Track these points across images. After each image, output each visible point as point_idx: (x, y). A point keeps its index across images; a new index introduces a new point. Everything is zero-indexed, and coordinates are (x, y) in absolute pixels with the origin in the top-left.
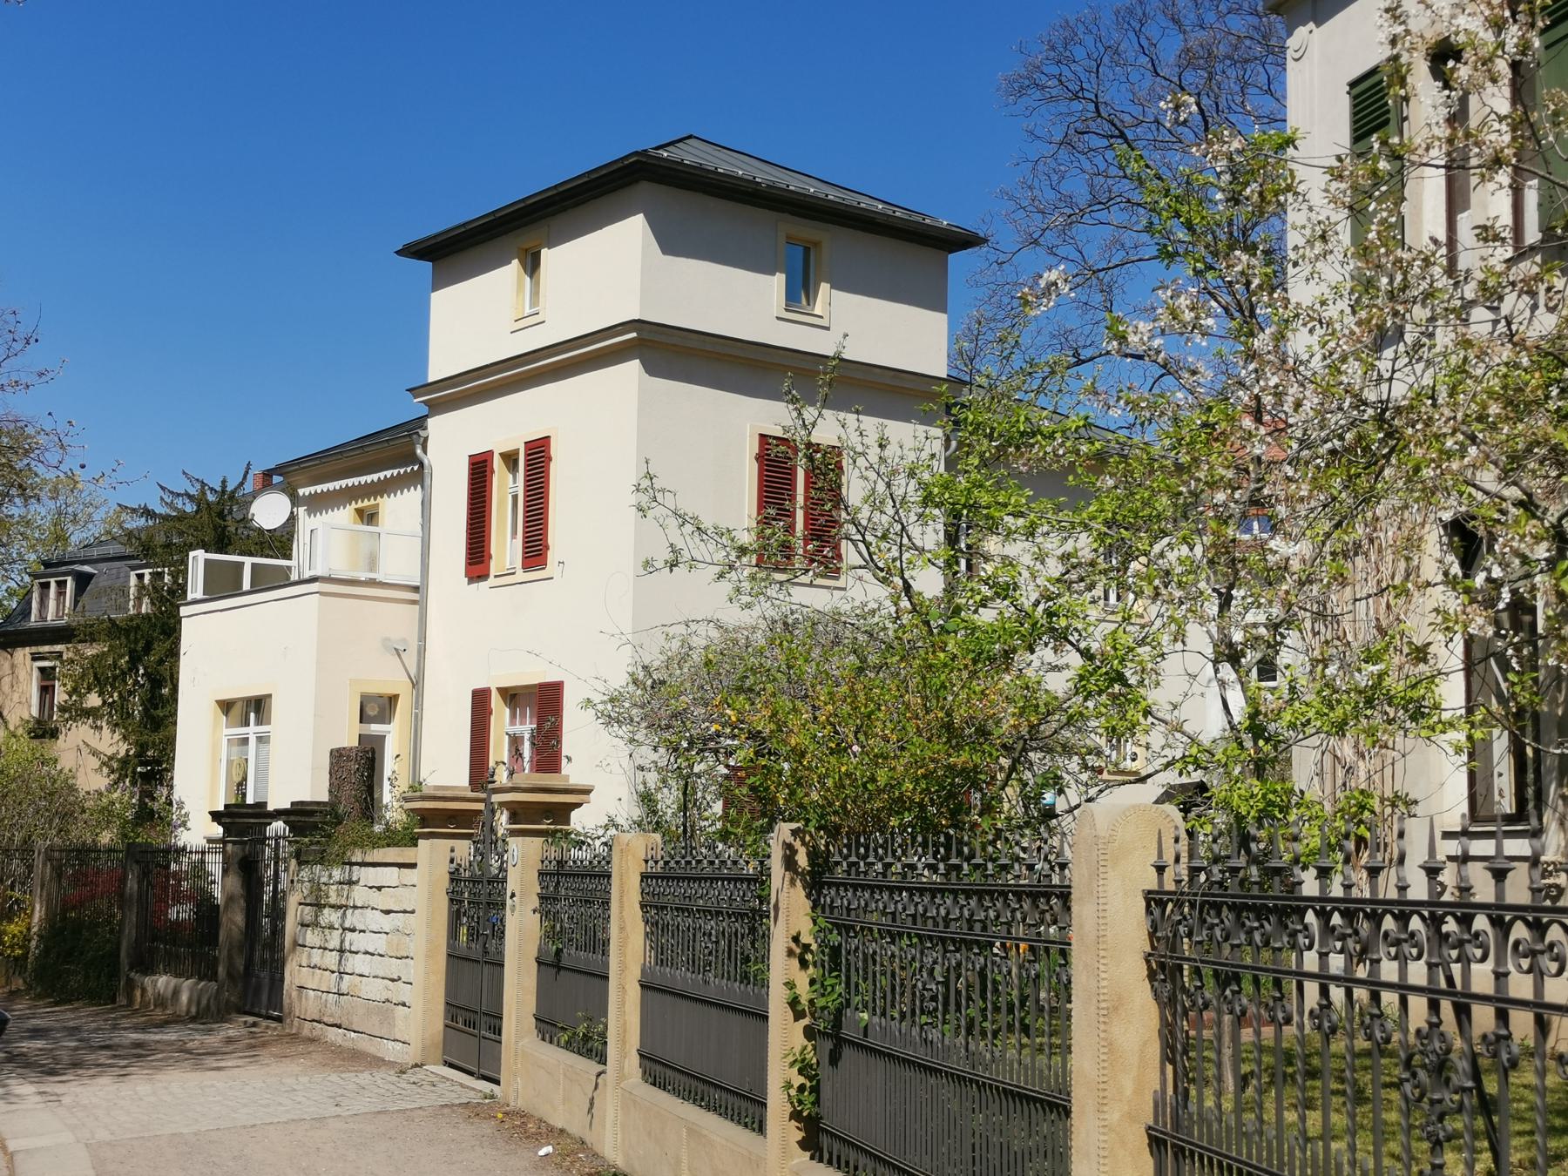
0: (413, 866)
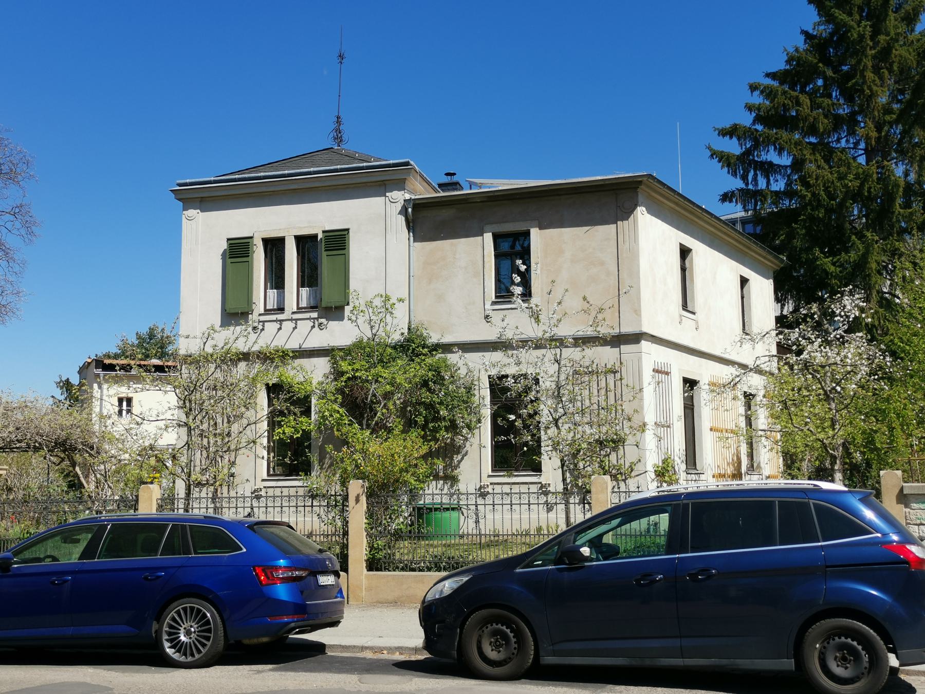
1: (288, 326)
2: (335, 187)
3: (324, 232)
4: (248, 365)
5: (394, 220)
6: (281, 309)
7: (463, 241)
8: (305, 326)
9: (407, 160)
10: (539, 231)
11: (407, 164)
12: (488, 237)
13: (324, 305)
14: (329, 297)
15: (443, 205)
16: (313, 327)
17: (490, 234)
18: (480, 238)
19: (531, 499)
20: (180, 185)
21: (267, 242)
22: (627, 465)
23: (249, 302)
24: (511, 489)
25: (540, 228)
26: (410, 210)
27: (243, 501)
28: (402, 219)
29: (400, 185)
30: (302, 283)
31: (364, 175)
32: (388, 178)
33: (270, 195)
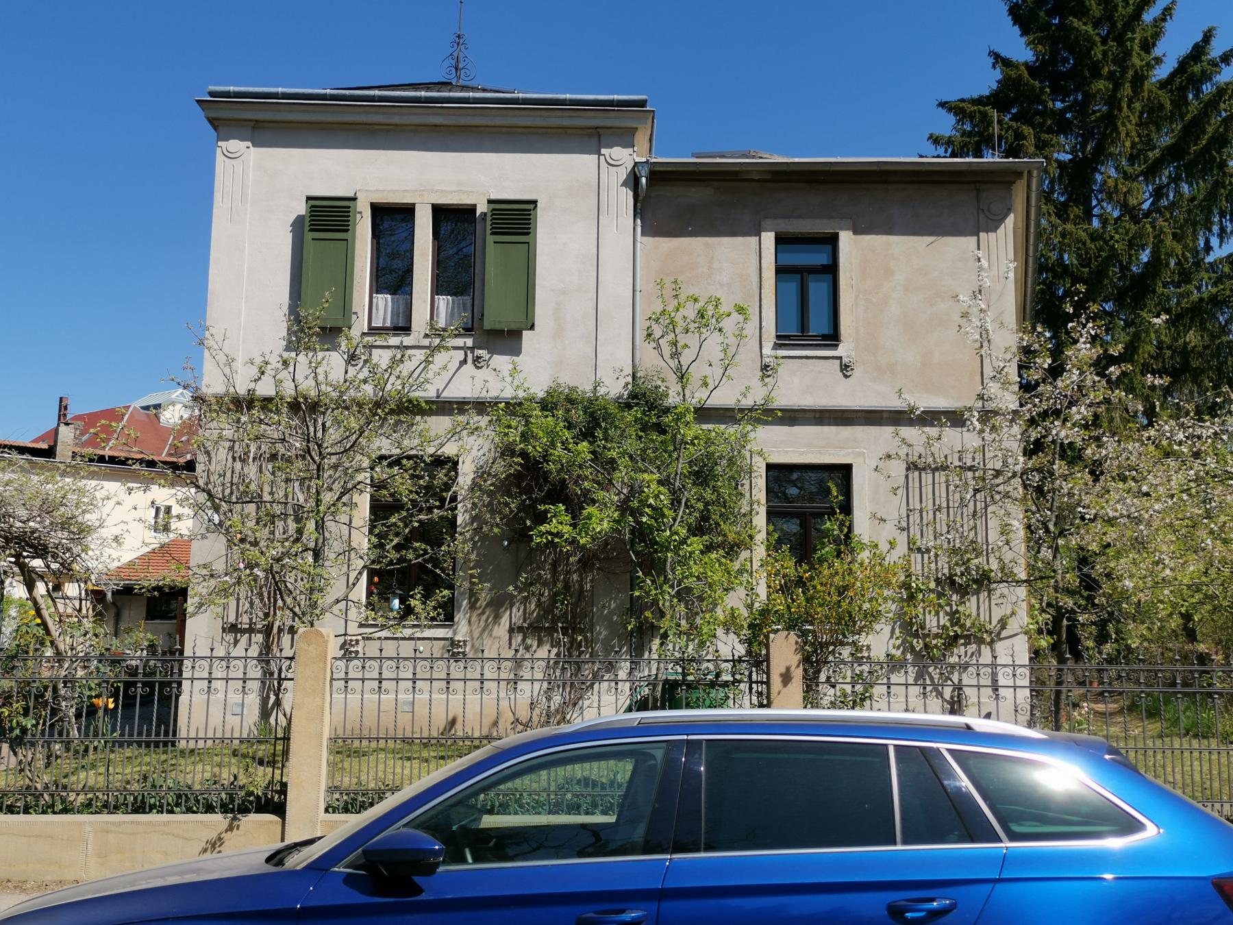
2: (509, 130)
3: (490, 202)
5: (613, 193)
6: (406, 329)
7: (726, 240)
8: (448, 359)
9: (644, 97)
10: (853, 236)
11: (642, 103)
12: (768, 238)
13: (487, 326)
14: (496, 314)
15: (695, 180)
16: (465, 361)
17: (773, 234)
20: (212, 94)
21: (381, 212)
22: (994, 622)
23: (345, 309)
25: (856, 232)
26: (644, 180)
27: (394, 666)
28: (627, 196)
29: (625, 137)
30: (439, 287)
31: (566, 113)
32: (608, 123)
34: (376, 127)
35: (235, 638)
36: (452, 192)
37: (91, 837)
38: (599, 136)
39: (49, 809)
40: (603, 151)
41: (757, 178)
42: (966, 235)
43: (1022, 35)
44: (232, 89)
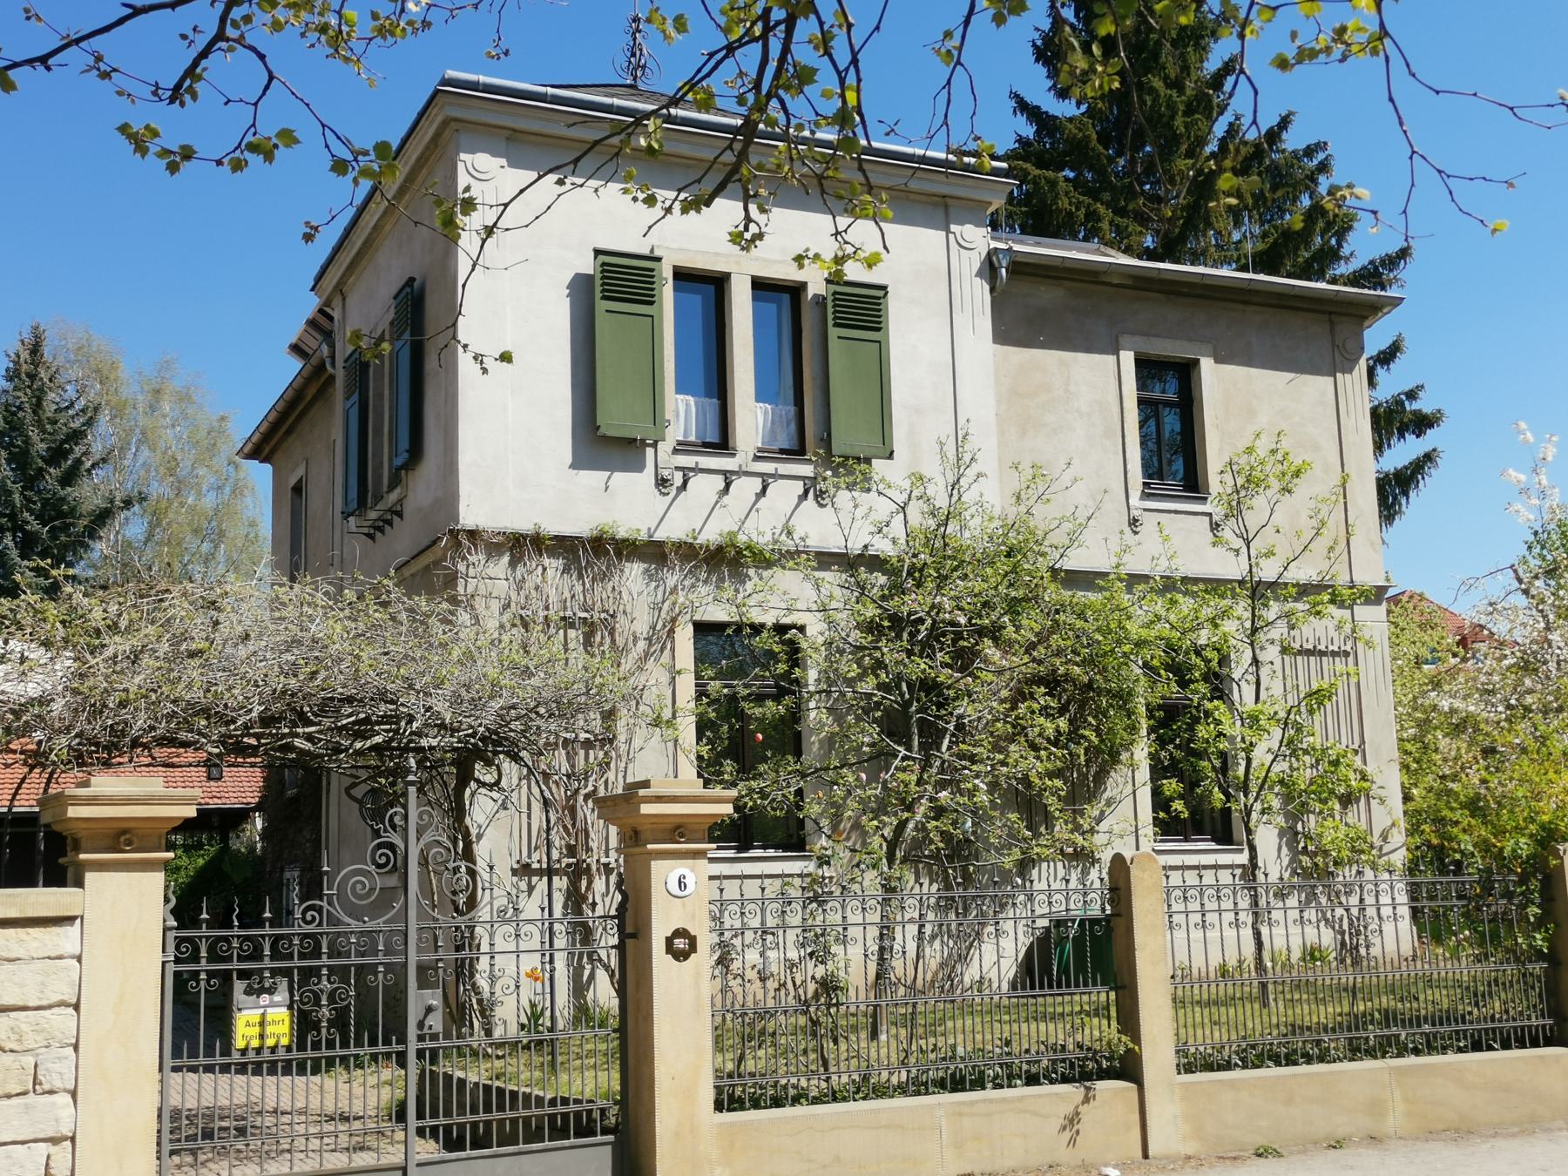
0: (68, 920)
1: (745, 488)
4: (647, 570)
12: (1128, 358)
18: (1325, 382)
19: (849, 913)
22: (1377, 832)
24: (722, 890)
28: (981, 290)
33: (689, 166)
34: (672, 159)
35: (529, 883)
36: (775, 262)
37: (944, 1123)
38: (946, 206)
39: (1309, 1059)
40: (953, 228)
41: (1115, 282)
42: (1323, 375)
43: (1048, 77)
44: (483, 79)
